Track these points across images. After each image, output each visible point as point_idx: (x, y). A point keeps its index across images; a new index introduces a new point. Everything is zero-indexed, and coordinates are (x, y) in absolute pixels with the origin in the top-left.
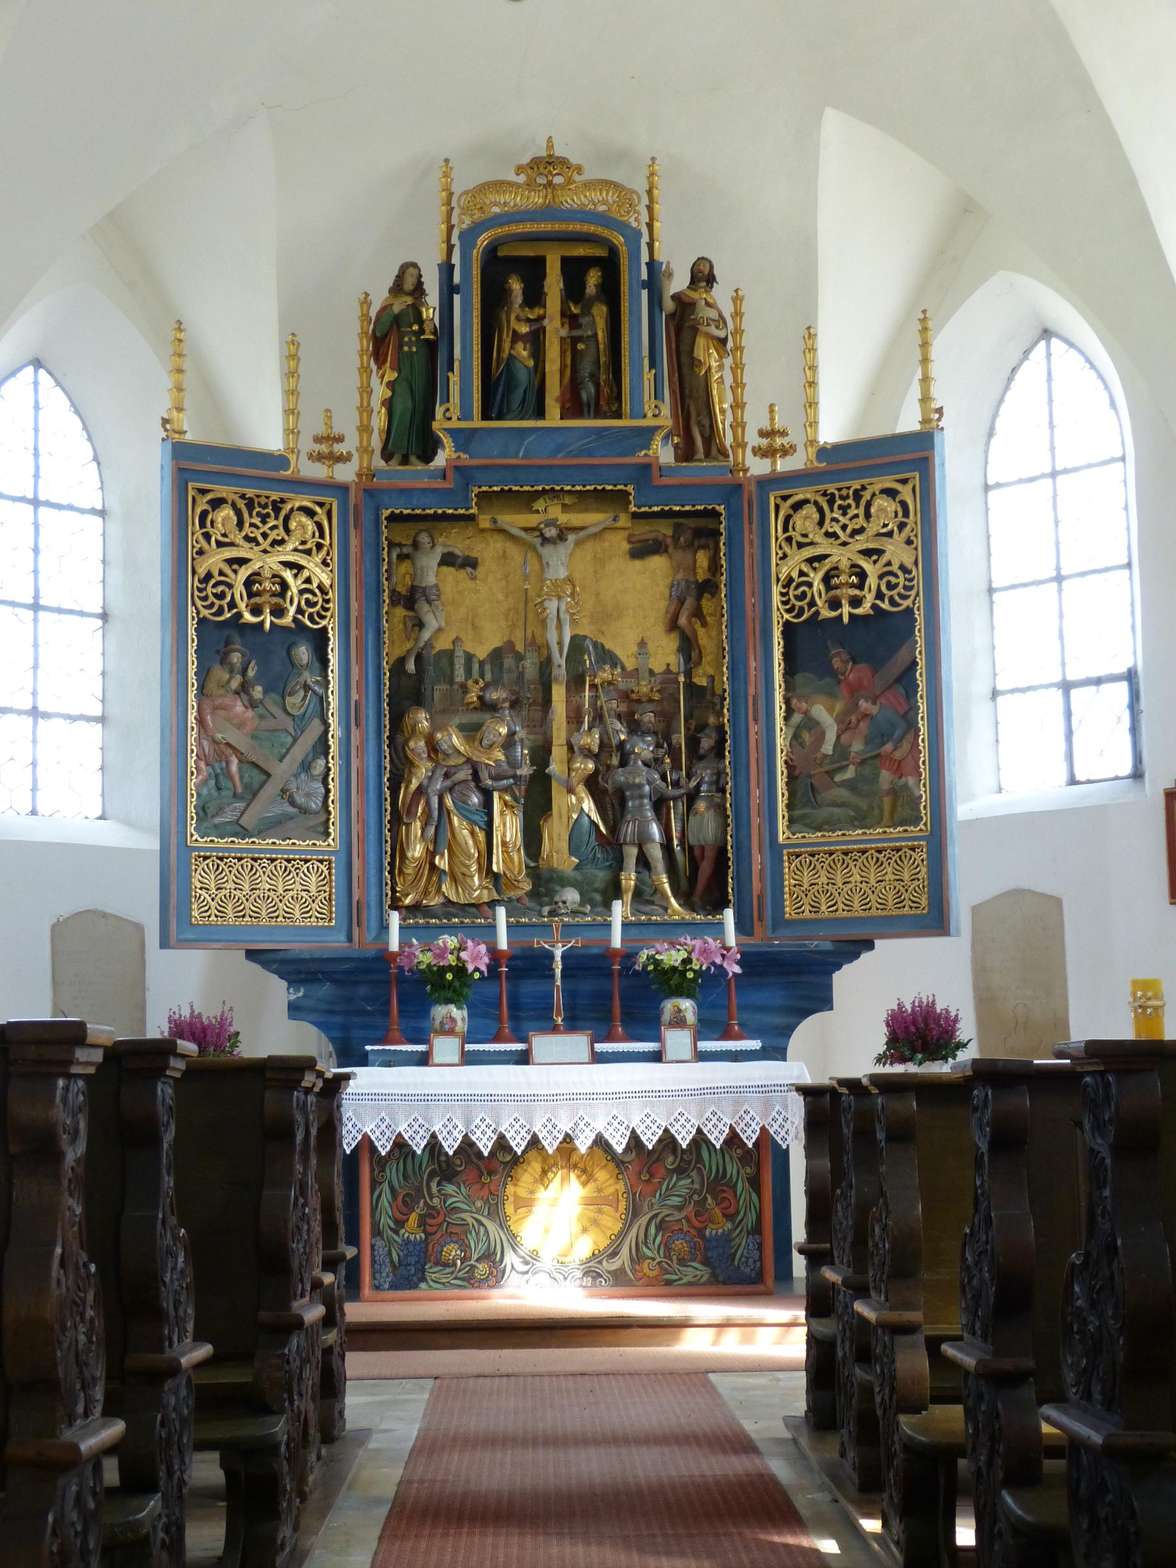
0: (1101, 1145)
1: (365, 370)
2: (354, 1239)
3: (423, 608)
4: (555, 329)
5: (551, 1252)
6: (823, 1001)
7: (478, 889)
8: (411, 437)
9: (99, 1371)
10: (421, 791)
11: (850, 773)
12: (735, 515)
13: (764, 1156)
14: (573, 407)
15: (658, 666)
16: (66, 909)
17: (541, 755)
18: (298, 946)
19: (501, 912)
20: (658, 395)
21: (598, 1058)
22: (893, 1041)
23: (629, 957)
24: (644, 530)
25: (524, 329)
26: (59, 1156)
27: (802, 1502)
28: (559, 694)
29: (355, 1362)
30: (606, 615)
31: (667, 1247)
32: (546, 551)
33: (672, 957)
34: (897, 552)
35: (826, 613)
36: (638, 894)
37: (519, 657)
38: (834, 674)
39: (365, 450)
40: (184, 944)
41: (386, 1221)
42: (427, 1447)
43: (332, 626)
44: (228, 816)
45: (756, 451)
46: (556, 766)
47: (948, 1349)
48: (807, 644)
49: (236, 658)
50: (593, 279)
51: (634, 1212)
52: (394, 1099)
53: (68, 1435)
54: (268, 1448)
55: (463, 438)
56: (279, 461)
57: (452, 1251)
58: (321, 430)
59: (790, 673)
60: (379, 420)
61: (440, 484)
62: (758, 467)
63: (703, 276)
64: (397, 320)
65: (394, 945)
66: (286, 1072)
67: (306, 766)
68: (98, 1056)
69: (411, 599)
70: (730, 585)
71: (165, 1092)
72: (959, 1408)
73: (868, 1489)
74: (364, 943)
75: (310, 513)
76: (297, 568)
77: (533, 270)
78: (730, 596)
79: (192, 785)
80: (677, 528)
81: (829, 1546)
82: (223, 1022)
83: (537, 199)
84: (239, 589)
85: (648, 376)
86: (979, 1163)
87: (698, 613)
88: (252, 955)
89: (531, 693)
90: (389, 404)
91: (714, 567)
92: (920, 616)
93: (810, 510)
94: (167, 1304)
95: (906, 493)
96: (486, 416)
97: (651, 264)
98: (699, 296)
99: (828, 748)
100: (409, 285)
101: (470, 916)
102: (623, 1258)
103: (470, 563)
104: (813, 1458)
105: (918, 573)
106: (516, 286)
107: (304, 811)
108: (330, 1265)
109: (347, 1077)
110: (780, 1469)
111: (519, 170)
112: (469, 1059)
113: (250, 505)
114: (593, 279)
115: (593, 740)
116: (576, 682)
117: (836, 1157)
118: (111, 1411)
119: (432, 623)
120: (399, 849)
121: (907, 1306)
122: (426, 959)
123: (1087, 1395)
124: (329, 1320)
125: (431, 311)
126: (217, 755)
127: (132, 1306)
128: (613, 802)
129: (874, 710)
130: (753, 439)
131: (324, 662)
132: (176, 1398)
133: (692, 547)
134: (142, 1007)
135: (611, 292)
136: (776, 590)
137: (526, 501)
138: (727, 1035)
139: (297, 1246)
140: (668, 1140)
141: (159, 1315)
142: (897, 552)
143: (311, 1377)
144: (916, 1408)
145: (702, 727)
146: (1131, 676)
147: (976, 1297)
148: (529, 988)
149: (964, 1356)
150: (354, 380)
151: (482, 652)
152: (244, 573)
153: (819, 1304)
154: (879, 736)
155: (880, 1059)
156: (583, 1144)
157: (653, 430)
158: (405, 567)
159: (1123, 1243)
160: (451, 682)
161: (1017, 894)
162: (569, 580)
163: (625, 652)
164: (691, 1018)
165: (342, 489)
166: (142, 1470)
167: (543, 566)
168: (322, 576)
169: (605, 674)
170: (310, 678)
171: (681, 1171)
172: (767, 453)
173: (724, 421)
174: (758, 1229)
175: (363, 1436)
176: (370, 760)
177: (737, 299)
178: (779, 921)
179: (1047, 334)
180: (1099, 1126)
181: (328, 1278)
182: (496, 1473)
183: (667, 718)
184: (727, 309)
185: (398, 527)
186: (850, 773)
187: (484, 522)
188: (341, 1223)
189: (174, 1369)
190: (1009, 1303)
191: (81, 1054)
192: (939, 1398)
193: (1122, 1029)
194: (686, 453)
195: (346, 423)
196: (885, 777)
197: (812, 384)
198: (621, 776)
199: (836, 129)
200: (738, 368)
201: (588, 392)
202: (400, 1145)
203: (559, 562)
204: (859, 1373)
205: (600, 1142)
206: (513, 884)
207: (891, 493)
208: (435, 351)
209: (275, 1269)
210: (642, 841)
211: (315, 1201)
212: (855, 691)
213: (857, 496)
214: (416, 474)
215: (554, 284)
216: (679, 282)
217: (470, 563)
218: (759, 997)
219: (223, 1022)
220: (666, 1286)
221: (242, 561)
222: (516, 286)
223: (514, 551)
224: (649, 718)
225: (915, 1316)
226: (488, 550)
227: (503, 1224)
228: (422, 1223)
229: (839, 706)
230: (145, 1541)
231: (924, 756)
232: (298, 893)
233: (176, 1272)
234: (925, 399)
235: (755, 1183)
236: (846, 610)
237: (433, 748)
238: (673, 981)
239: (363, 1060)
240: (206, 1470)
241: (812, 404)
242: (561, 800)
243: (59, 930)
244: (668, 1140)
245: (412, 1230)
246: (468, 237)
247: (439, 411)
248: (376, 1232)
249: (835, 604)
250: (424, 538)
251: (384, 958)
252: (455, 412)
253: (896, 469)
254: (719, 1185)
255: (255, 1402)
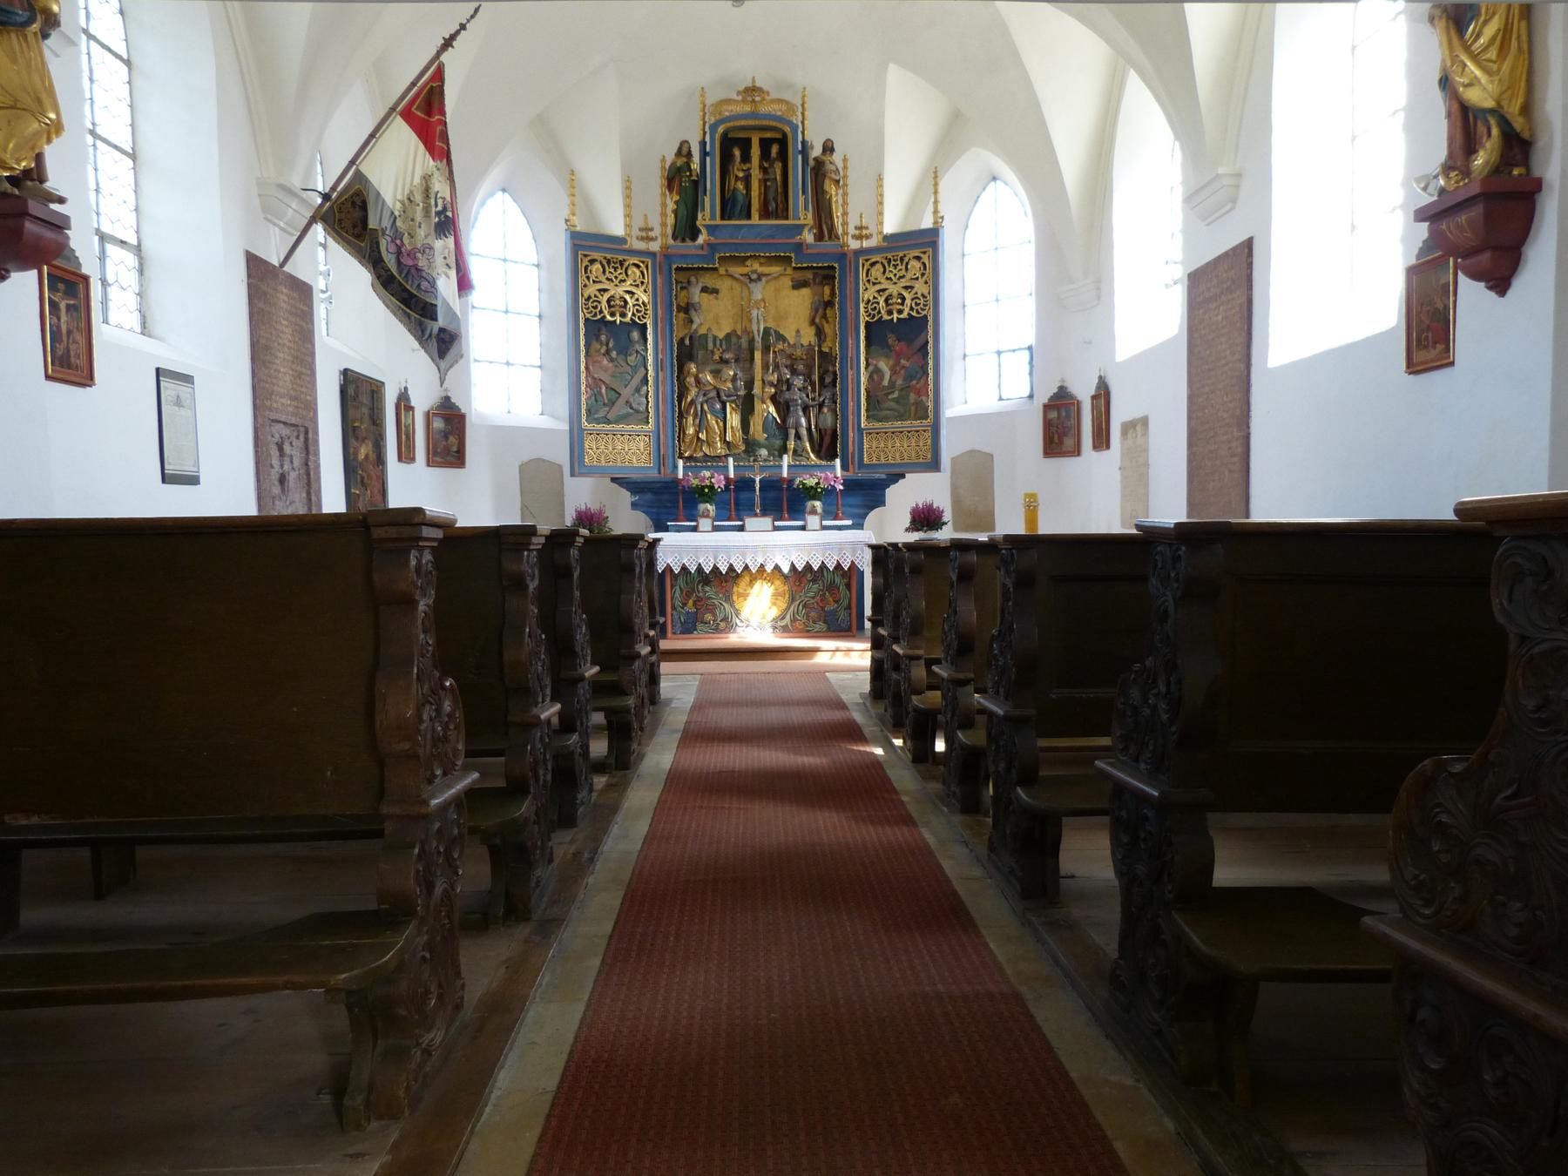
0: (1009, 582)
1: (664, 195)
2: (663, 614)
3: (693, 313)
4: (756, 175)
5: (757, 617)
6: (880, 502)
7: (720, 449)
8: (686, 228)
9: (548, 681)
10: (692, 402)
11: (896, 395)
12: (843, 269)
13: (850, 575)
14: (765, 214)
15: (805, 341)
16: (526, 458)
17: (749, 385)
18: (635, 476)
19: (731, 460)
20: (806, 208)
21: (776, 529)
22: (913, 521)
23: (790, 481)
24: (799, 275)
25: (741, 175)
26: (527, 587)
27: (867, 731)
28: (758, 355)
29: (665, 667)
30: (780, 317)
31: (807, 615)
32: (752, 286)
33: (811, 482)
34: (920, 287)
35: (886, 317)
36: (795, 452)
37: (739, 337)
38: (889, 347)
39: (664, 235)
40: (581, 475)
41: (678, 603)
42: (698, 707)
43: (649, 322)
44: (600, 415)
45: (854, 237)
46: (757, 391)
47: (935, 668)
48: (877, 332)
49: (603, 338)
50: (775, 149)
51: (793, 599)
52: (680, 548)
53: (535, 711)
54: (628, 711)
55: (712, 229)
56: (622, 240)
57: (708, 617)
58: (642, 225)
59: (868, 346)
60: (671, 220)
61: (700, 252)
62: (854, 245)
63: (828, 148)
64: (679, 170)
65: (680, 476)
66: (632, 540)
67: (638, 390)
68: (543, 540)
69: (687, 309)
70: (840, 303)
71: (574, 553)
72: (939, 693)
73: (897, 726)
74: (666, 474)
75: (638, 266)
76: (632, 293)
77: (745, 145)
78: (840, 309)
79: (583, 398)
80: (815, 275)
81: (879, 751)
82: (601, 512)
83: (748, 109)
84: (604, 304)
85: (801, 198)
86: (952, 586)
87: (824, 316)
88: (614, 480)
89: (745, 355)
90: (675, 212)
91: (833, 294)
92: (930, 319)
93: (879, 266)
94: (578, 649)
95: (925, 258)
96: (722, 218)
97: (804, 142)
98: (826, 158)
99: (886, 383)
100: (685, 151)
101: (716, 461)
102: (787, 620)
103: (715, 291)
104: (873, 712)
105: (930, 298)
106: (737, 153)
107: (637, 411)
108: (652, 626)
109: (657, 541)
110: (858, 717)
111: (739, 93)
112: (716, 529)
113: (609, 262)
114: (775, 149)
115: (774, 378)
116: (766, 349)
117: (886, 578)
118: (554, 699)
119: (697, 321)
120: (682, 429)
121: (918, 648)
122: (695, 482)
123: (997, 693)
124: (653, 652)
125: (695, 166)
126: (594, 384)
127: (562, 651)
128: (784, 408)
129: (907, 364)
130: (852, 231)
131: (645, 339)
132: (583, 690)
133: (822, 284)
134: (562, 504)
135: (783, 156)
136: (862, 306)
137: (742, 261)
138: (836, 518)
139: (637, 621)
140: (808, 567)
141: (574, 654)
142: (920, 287)
143: (645, 678)
144: (919, 693)
145: (826, 372)
146: (1030, 348)
147: (949, 646)
148: (744, 496)
149: (941, 671)
150: (658, 200)
151: (721, 335)
152: (606, 296)
153: (877, 644)
154: (910, 377)
155: (907, 530)
156: (769, 568)
157: (803, 226)
158: (684, 293)
159: (996, 798)
160: (706, 349)
161: (972, 452)
162: (763, 300)
163: (790, 335)
164: (819, 510)
165: (653, 255)
166: (568, 724)
167: (751, 293)
168: (644, 298)
169: (780, 346)
170: (639, 347)
171: (814, 581)
172: (859, 237)
173: (838, 222)
174: (849, 607)
175: (669, 701)
176: (669, 387)
177: (845, 160)
178: (861, 465)
179: (994, 179)
180: (1008, 573)
181: (652, 633)
182: (728, 719)
183: (810, 367)
184: (840, 165)
185: (679, 274)
186: (896, 395)
187: (722, 271)
188: (657, 607)
189: (582, 679)
190: (963, 648)
191: (535, 540)
192: (931, 688)
193: (1019, 528)
194: (819, 237)
195: (655, 222)
196: (912, 397)
197: (881, 203)
198: (787, 395)
199: (894, 73)
200: (845, 194)
201: (772, 206)
202: (684, 568)
203: (758, 291)
204: (894, 676)
205: (777, 568)
206: (736, 447)
207: (918, 258)
208: (697, 186)
209: (627, 630)
210: (797, 426)
211: (645, 598)
212: (899, 356)
213: (902, 259)
214: (689, 247)
215: (755, 152)
216: (817, 151)
217: (715, 291)
218: (851, 500)
219: (601, 512)
220: (807, 633)
221: (605, 290)
222: (737, 153)
223: (736, 285)
224: (801, 367)
225: (920, 652)
226: (724, 285)
227: (732, 605)
228: (695, 604)
229: (891, 362)
230: (572, 753)
231: (931, 387)
232: (634, 450)
233: (582, 634)
234: (936, 212)
235: (848, 586)
236: (895, 315)
237: (698, 381)
238: (812, 493)
239: (666, 529)
240: (598, 718)
241: (881, 213)
242: (758, 406)
243: (523, 468)
244: (808, 567)
245: (690, 607)
246: (713, 128)
247: (700, 216)
248: (673, 608)
249: (890, 313)
250: (693, 279)
251: (676, 481)
252: (708, 216)
253: (920, 246)
254: (832, 587)
255: (617, 690)
